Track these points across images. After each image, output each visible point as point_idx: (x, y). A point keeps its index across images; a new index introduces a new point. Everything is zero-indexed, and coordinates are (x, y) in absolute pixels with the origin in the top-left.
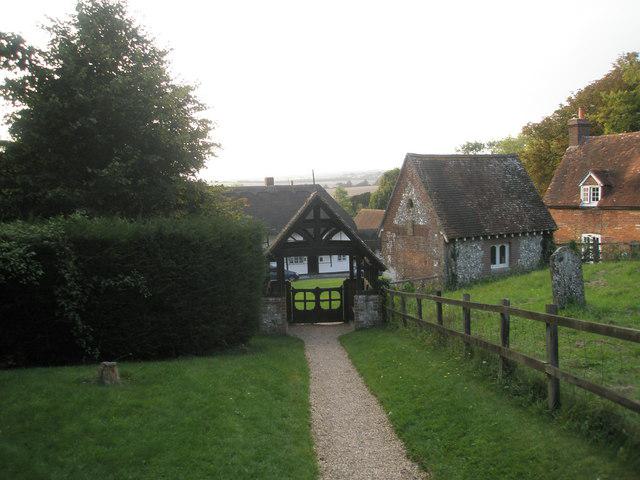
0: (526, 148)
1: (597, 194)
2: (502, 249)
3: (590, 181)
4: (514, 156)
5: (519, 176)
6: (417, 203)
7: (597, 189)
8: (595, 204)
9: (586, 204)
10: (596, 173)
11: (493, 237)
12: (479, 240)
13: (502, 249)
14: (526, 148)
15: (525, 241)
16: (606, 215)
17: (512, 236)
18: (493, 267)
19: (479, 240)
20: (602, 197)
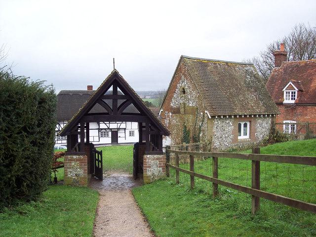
0: (265, 67)
1: (295, 96)
2: (245, 125)
3: (291, 88)
4: (251, 65)
5: (255, 77)
6: (188, 91)
7: (295, 93)
8: (293, 102)
9: (285, 102)
10: (294, 83)
11: (240, 116)
12: (261, 117)
13: (245, 125)
14: (265, 67)
15: (260, 121)
16: (299, 110)
17: (251, 118)
18: (239, 138)
19: (261, 117)
20: (297, 98)
